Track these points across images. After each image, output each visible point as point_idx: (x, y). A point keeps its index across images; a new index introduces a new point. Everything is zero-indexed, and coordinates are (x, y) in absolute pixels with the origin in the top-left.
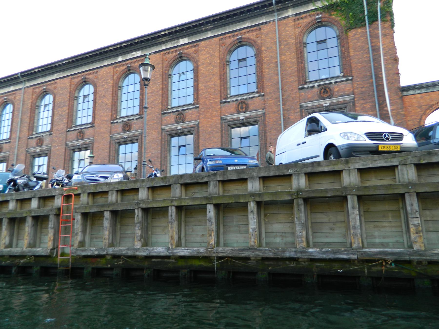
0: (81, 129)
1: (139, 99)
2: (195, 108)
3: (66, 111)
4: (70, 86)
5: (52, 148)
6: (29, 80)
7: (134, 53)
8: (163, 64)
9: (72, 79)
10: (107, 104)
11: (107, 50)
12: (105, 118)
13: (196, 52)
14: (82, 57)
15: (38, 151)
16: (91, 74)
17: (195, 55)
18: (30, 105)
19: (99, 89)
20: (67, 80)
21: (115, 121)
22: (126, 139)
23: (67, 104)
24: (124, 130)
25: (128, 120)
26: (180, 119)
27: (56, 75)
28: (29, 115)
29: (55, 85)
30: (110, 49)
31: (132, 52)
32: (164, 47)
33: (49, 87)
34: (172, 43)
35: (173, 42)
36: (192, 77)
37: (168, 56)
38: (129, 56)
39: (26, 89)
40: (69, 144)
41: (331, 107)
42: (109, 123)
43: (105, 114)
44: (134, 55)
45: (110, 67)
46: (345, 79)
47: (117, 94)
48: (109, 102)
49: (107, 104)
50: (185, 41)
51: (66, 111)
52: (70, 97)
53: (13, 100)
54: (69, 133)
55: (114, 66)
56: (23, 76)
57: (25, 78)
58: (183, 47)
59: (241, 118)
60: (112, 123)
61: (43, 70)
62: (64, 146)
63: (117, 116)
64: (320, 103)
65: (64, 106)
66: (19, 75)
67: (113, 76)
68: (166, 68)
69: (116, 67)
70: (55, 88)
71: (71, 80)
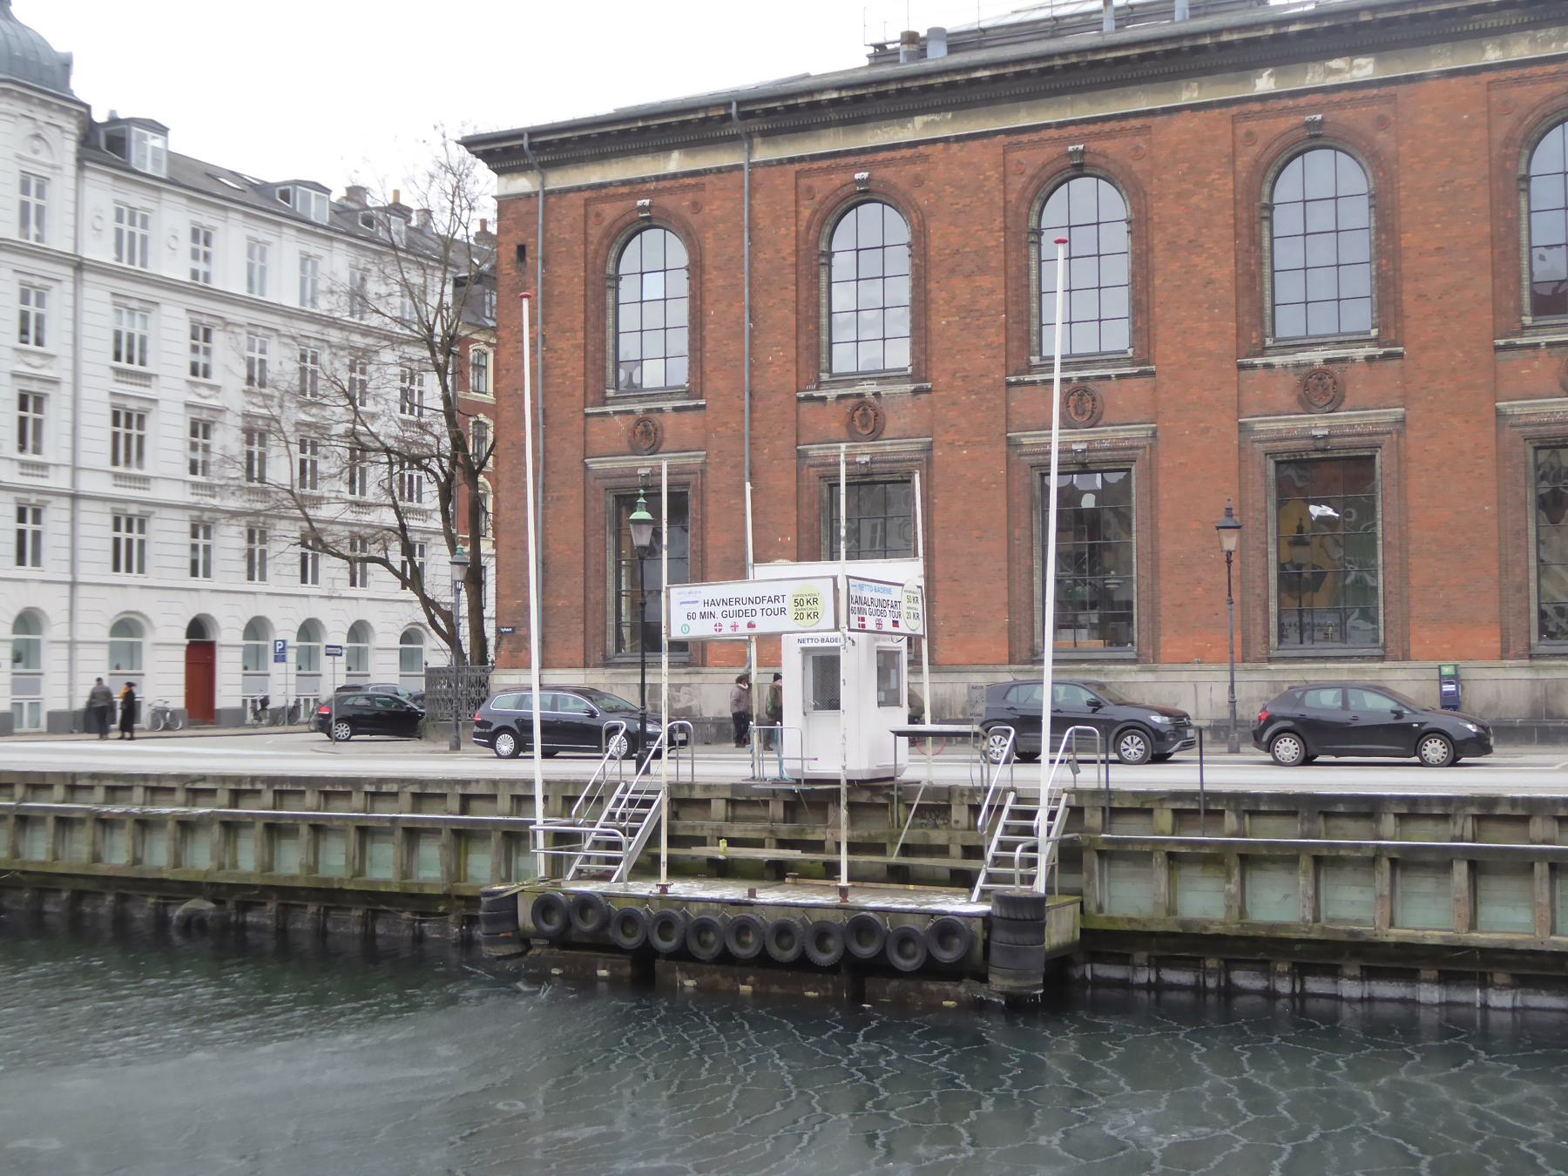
0: (1081, 379)
1: (1125, 292)
2: (1387, 356)
3: (992, 292)
4: (1004, 178)
5: (938, 453)
6: (768, 135)
7: (1336, 63)
8: (1489, 127)
9: (587, 202)
10: (1210, 282)
11: (1208, 41)
12: (1210, 345)
13: (696, 207)
14: (1074, 60)
15: (642, 472)
16: (1110, 135)
17: (362, 262)
18: (788, 248)
19: (937, 231)
20: (984, 155)
21: (1258, 361)
22: (1321, 444)
23: (996, 260)
24: (1306, 404)
25: (1327, 361)
26: (865, 426)
27: (919, 121)
28: (790, 294)
29: (918, 168)
30: (1225, 38)
31: (1331, 58)
32: (1493, 55)
33: (887, 173)
34: (1533, 40)
35: (1541, 34)
36: (686, 293)
37: (1515, 93)
38: (1314, 77)
39: (552, 199)
40: (1025, 441)
41: (1335, 440)
42: (1229, 365)
43: (1205, 326)
44: (1339, 71)
45: (1470, 80)
46: (1136, 370)
47: (1255, 241)
48: (1224, 273)
49: (1210, 282)
50: (1364, 68)
51: (992, 292)
52: (1006, 228)
53: (688, 215)
54: (1016, 391)
55: (1235, 110)
56: (745, 116)
57: (755, 125)
58: (1123, 124)
59: (1074, 447)
60: (1241, 367)
61: (857, 99)
62: (1003, 448)
63: (1263, 336)
64: (628, 464)
65: (982, 270)
66: (525, 142)
67: (1234, 157)
68: (1507, 146)
69: (1247, 116)
70: (918, 181)
71: (1005, 153)
